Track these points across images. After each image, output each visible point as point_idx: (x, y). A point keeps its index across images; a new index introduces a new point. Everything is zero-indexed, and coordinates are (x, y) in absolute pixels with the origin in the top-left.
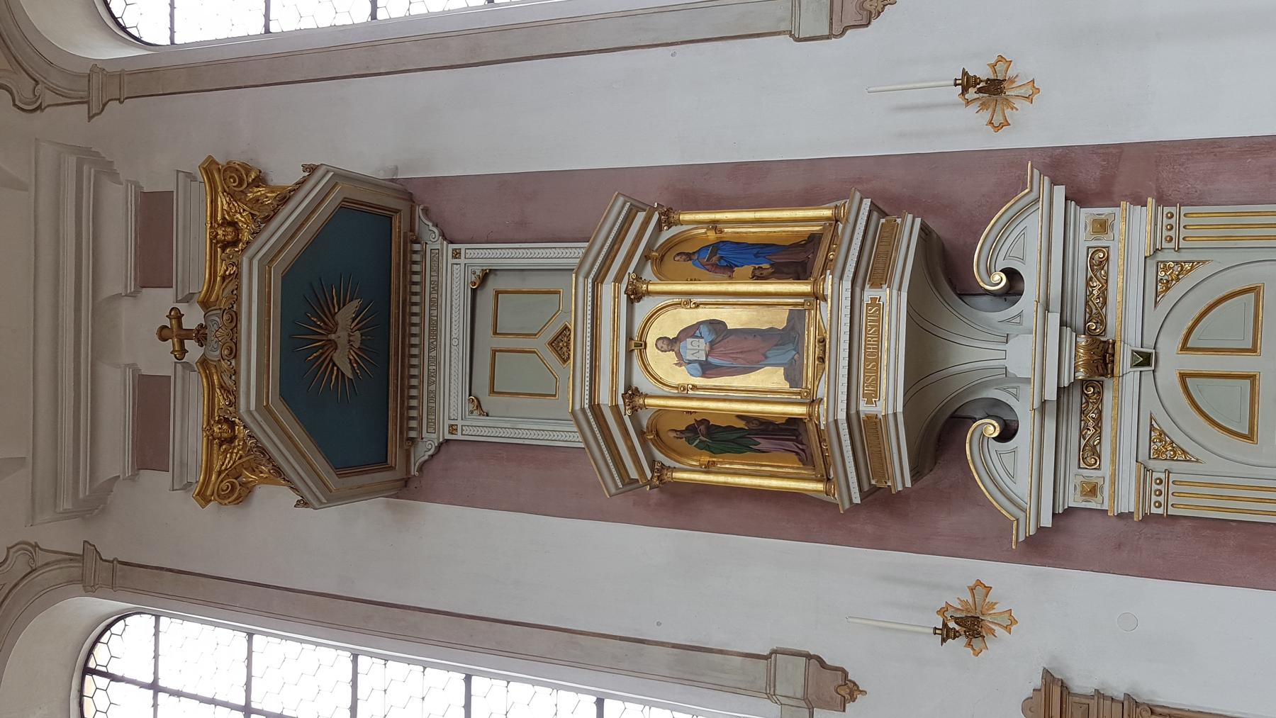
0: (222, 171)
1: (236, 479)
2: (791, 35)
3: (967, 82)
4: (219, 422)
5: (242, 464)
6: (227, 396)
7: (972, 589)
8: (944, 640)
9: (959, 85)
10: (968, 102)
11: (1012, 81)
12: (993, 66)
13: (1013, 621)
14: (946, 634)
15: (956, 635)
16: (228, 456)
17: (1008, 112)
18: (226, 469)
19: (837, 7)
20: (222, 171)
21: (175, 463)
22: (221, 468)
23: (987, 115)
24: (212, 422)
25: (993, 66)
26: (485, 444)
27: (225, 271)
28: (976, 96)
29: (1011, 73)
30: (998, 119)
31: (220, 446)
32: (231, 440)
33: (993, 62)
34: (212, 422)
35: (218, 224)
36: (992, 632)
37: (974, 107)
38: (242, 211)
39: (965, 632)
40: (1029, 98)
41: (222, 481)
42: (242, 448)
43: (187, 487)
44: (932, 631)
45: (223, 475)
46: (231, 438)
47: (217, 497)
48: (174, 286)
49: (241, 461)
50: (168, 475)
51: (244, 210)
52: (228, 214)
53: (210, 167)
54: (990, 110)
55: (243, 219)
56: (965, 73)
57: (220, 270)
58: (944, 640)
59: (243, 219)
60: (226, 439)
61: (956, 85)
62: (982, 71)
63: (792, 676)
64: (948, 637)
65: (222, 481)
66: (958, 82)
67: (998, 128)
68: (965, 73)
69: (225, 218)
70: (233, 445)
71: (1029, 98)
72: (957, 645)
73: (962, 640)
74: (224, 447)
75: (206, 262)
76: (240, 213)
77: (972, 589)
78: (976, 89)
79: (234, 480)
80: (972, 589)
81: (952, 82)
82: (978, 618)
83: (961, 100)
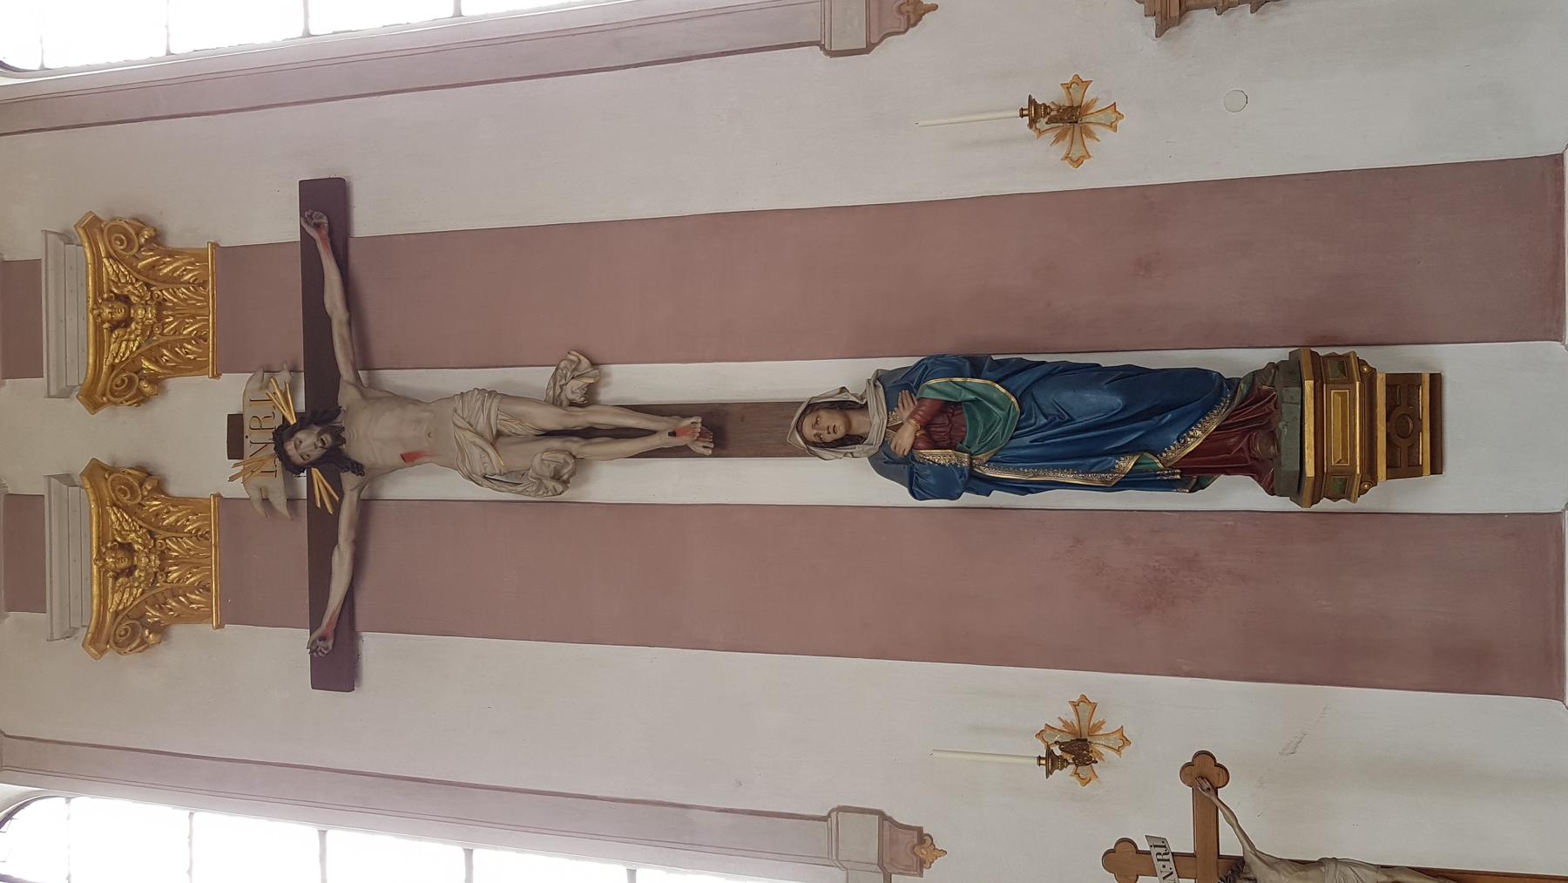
0: (106, 231)
1: (136, 373)
2: (822, 47)
3: (1035, 112)
4: (109, 299)
5: (140, 354)
6: (122, 515)
7: (1075, 706)
8: (1049, 773)
9: (1026, 115)
10: (1040, 132)
11: (1088, 106)
12: (1068, 87)
13: (1126, 742)
14: (1052, 762)
15: (1064, 763)
16: (123, 345)
17: (1088, 141)
18: (124, 609)
19: (874, 6)
20: (106, 231)
21: (51, 363)
22: (114, 360)
23: (1062, 149)
24: (104, 550)
25: (1068, 87)
26: (463, 365)
27: (119, 605)
28: (1048, 126)
29: (1089, 95)
30: (1075, 155)
31: (116, 578)
32: (129, 571)
33: (1068, 81)
34: (104, 550)
35: (103, 299)
36: (1100, 755)
37: (1051, 136)
38: (134, 280)
39: (1073, 759)
40: (1112, 126)
41: (116, 376)
42: (142, 333)
43: (65, 394)
44: (1036, 761)
45: (120, 617)
46: (129, 568)
47: (114, 645)
48: (45, 375)
49: (139, 351)
50: (39, 382)
51: (137, 280)
52: (119, 533)
53: (92, 225)
54: (1068, 139)
55: (136, 292)
56: (1032, 101)
57: (112, 604)
58: (1049, 773)
59: (136, 292)
60: (123, 571)
61: (1022, 116)
62: (1052, 94)
63: (862, 841)
64: (1054, 767)
65: (116, 376)
66: (1025, 112)
67: (1077, 162)
68: (1032, 101)
69: (112, 292)
70: (128, 330)
71: (1112, 126)
72: (1064, 776)
73: (1071, 768)
74: (120, 580)
75: (87, 277)
76: (132, 284)
77: (1075, 705)
78: (1046, 120)
79: (136, 622)
80: (1075, 705)
81: (1018, 114)
82: (1086, 740)
83: (1031, 132)
